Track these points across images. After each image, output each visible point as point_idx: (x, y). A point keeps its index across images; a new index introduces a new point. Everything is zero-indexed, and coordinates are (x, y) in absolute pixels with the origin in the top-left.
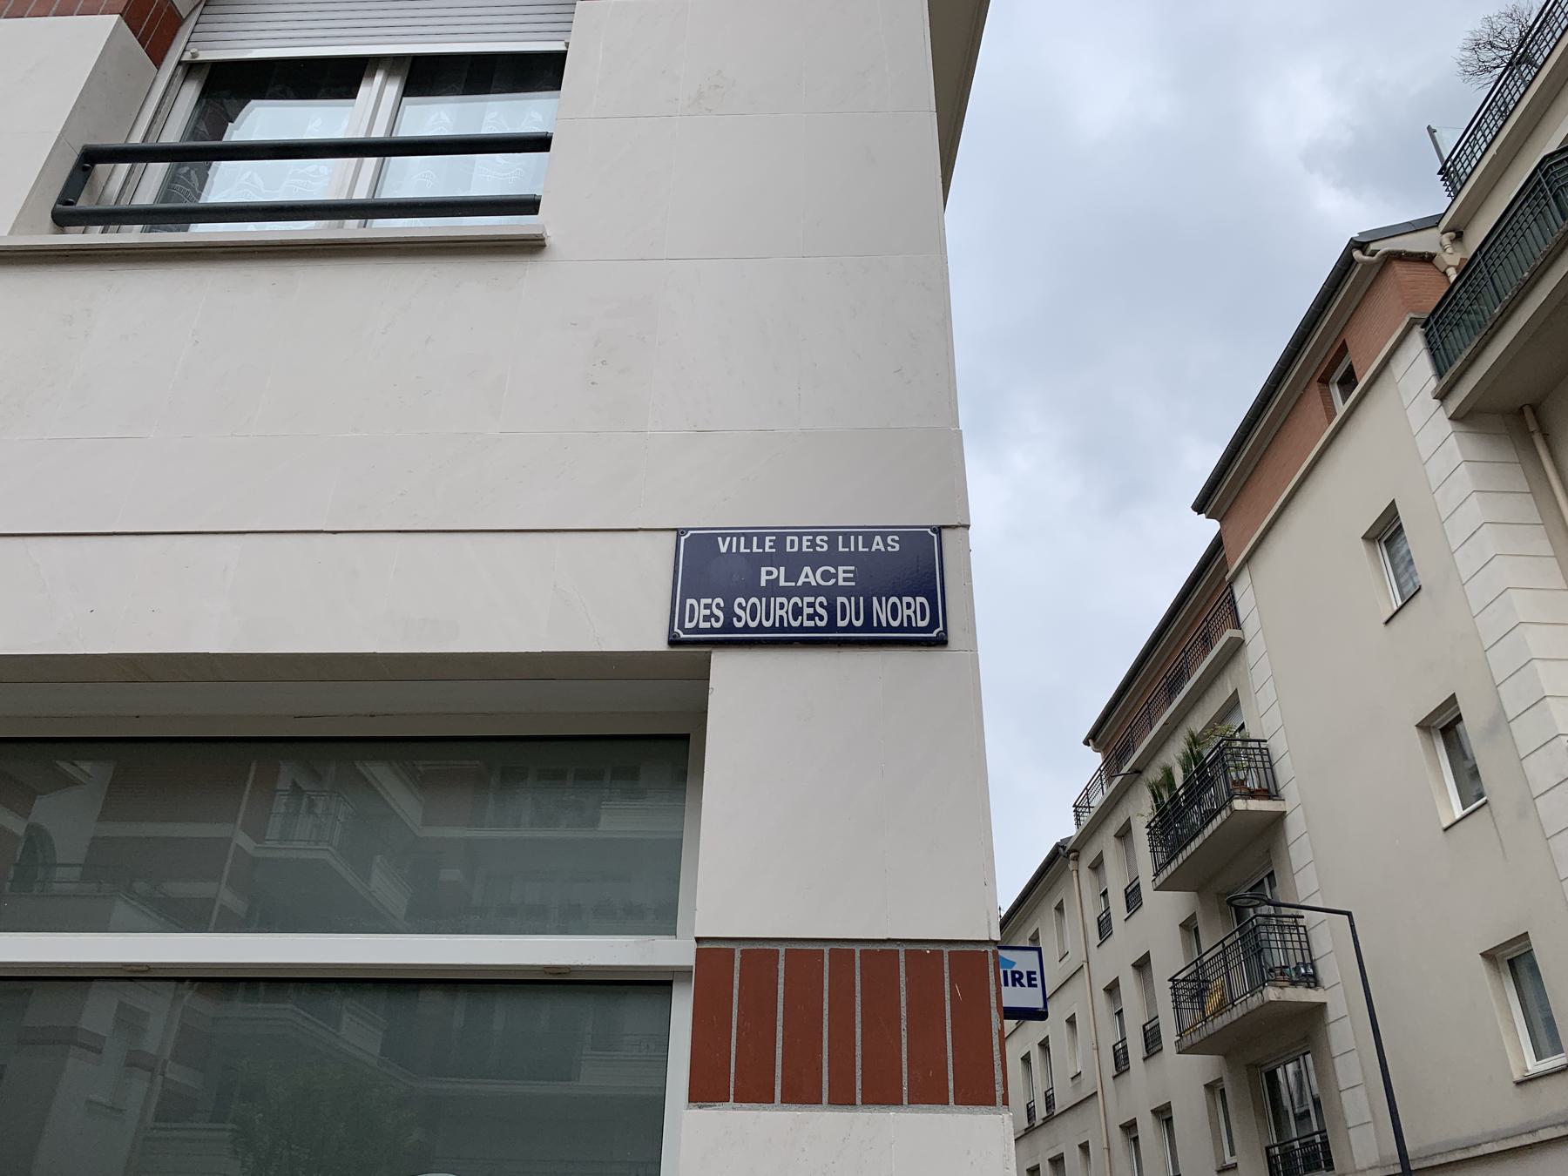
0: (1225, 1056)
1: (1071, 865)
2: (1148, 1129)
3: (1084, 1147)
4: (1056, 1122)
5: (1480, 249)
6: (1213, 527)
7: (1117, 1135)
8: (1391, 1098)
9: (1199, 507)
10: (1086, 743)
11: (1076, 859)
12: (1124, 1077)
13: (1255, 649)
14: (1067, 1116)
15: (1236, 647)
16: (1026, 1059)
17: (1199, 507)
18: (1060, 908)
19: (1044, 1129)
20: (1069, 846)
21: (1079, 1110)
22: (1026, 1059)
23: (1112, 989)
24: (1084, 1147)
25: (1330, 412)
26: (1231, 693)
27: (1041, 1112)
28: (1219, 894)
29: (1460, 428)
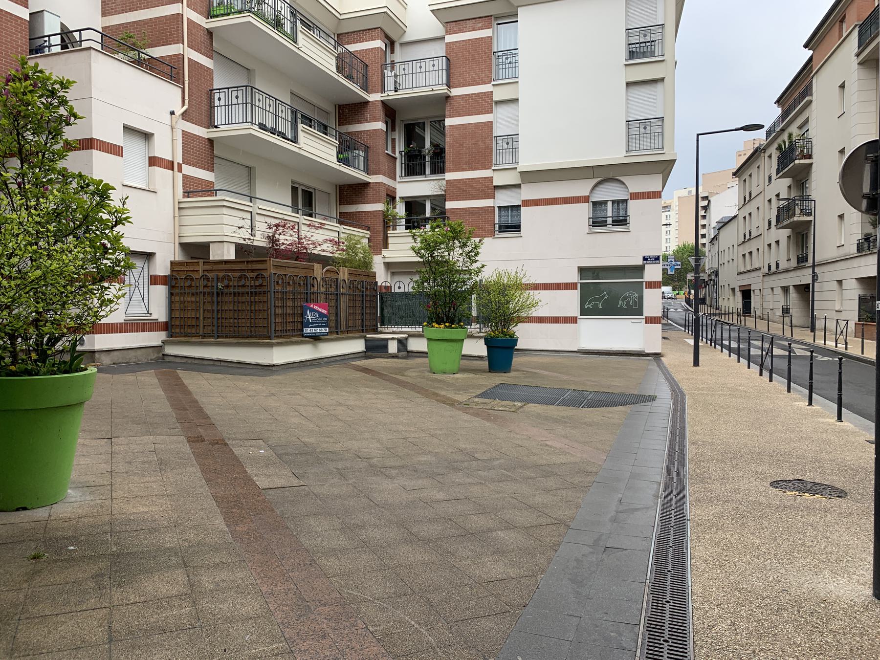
0: (792, 229)
1: (762, 155)
2: (747, 255)
3: (758, 249)
4: (751, 241)
5: (870, 14)
6: (811, 52)
7: (766, 247)
8: (295, 365)
9: (806, 46)
10: (775, 103)
11: (765, 152)
12: (770, 230)
13: (814, 104)
14: (754, 239)
15: (810, 102)
16: (745, 218)
17: (806, 46)
18: (758, 167)
19: (747, 243)
20: (762, 148)
21: (758, 238)
22: (745, 218)
23: (770, 201)
24: (758, 249)
25: (840, 35)
26: (876, 5)
27: (747, 237)
28: (797, 181)
29: (860, 67)
